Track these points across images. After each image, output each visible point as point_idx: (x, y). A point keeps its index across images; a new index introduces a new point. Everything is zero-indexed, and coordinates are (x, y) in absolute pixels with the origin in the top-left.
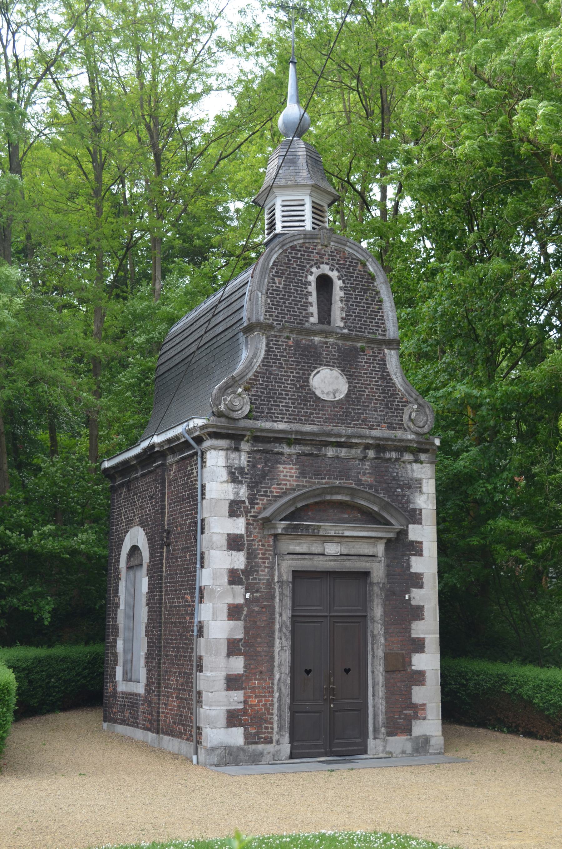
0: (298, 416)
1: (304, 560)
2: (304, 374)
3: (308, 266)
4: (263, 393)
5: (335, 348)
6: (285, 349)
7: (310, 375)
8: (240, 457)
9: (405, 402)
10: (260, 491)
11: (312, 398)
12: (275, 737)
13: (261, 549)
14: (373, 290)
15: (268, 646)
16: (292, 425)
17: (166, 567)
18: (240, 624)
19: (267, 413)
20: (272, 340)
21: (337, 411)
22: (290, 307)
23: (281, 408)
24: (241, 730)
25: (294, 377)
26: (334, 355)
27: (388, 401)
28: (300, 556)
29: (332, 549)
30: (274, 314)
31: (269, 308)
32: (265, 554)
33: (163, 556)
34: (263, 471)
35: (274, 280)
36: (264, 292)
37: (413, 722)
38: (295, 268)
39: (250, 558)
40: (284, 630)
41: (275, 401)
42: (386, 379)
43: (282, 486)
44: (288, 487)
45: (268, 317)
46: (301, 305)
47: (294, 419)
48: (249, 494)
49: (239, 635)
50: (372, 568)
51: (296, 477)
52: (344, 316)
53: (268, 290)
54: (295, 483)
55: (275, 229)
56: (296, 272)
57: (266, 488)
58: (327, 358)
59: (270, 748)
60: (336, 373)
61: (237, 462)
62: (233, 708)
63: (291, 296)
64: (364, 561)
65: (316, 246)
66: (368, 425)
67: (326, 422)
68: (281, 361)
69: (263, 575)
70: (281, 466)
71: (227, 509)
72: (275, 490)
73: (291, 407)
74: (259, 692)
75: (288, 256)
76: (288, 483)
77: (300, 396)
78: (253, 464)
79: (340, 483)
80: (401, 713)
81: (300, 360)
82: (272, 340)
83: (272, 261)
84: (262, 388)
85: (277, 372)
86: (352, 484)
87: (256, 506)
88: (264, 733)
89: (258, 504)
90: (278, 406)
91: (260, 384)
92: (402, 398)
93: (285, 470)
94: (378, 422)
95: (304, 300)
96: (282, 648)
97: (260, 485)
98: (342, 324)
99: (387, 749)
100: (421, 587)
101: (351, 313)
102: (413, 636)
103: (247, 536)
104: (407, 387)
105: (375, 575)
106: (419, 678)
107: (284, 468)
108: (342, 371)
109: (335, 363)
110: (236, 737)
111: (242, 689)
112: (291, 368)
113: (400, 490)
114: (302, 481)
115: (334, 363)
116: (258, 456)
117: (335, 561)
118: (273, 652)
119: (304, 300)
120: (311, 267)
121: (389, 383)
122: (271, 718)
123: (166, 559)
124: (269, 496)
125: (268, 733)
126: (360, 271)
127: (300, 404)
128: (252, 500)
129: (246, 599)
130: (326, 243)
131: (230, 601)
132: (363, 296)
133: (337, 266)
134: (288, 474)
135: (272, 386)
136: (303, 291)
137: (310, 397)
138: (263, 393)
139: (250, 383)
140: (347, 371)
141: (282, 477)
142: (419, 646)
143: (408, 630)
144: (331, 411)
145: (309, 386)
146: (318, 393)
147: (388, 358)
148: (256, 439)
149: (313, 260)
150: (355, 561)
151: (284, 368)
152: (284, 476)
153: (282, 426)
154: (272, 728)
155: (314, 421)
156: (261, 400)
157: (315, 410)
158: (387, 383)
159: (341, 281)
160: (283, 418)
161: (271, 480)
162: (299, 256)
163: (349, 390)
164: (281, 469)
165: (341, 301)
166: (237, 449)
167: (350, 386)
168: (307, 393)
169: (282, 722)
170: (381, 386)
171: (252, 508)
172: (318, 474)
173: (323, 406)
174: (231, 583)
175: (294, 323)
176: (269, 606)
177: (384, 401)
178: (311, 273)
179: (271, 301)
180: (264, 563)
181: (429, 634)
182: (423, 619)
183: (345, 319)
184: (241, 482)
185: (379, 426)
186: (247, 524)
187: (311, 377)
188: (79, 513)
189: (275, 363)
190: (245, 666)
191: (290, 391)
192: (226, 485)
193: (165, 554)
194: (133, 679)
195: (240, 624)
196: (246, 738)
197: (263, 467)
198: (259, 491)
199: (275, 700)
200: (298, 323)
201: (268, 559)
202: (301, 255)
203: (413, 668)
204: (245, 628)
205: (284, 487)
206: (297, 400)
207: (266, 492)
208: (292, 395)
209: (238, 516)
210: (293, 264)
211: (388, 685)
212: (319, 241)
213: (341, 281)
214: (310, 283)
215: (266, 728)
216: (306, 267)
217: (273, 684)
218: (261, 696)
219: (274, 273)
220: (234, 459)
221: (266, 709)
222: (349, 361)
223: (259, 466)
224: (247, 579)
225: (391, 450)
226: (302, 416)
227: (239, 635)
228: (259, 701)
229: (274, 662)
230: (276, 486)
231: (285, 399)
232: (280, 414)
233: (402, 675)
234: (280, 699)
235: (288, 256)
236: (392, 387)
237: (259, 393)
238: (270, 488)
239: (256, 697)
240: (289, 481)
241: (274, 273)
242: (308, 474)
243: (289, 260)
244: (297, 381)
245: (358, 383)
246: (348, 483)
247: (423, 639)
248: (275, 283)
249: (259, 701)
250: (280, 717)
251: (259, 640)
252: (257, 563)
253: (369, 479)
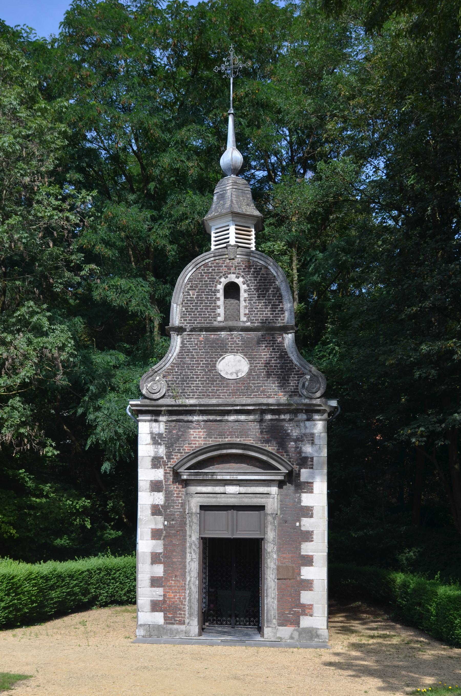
0: (206, 392)
1: (209, 497)
2: (211, 361)
3: (217, 277)
4: (178, 378)
5: (239, 338)
6: (197, 344)
7: (216, 361)
8: (159, 426)
9: (301, 374)
10: (175, 450)
11: (218, 378)
12: (187, 621)
13: (176, 491)
16: (200, 400)
18: (161, 542)
19: (181, 393)
20: (186, 339)
21: (239, 387)
22: (201, 312)
23: (192, 388)
24: (162, 614)
25: (203, 364)
26: (238, 344)
27: (285, 375)
28: (205, 495)
30: (188, 319)
31: (184, 314)
32: (179, 494)
35: (189, 292)
36: (179, 303)
37: (301, 617)
38: (207, 281)
39: (168, 496)
40: (194, 547)
42: (284, 357)
43: (192, 445)
44: (197, 445)
45: (183, 321)
46: (211, 309)
47: (203, 395)
48: (167, 452)
49: (160, 550)
50: (267, 503)
52: (247, 312)
53: (184, 301)
54: (203, 443)
56: (207, 284)
57: (179, 447)
58: (232, 347)
59: (183, 627)
60: (239, 357)
61: (157, 429)
63: (202, 303)
64: (259, 498)
65: (224, 261)
66: (266, 395)
67: (230, 395)
68: (193, 353)
69: (178, 509)
70: (192, 431)
71: (150, 463)
73: (200, 387)
74: (175, 589)
75: (201, 273)
76: (197, 443)
77: (208, 378)
78: (169, 431)
79: (240, 441)
80: (291, 610)
81: (209, 351)
82: (186, 339)
83: (187, 278)
84: (177, 375)
85: (189, 362)
86: (251, 440)
87: (172, 460)
88: (179, 617)
89: (173, 458)
90: (191, 387)
91: (176, 372)
92: (298, 371)
93: (195, 434)
94: (276, 392)
95: (213, 305)
96: (192, 559)
97: (175, 445)
98: (245, 319)
99: (278, 636)
100: (312, 517)
101: (254, 309)
102: (302, 553)
103: (165, 482)
104: (302, 362)
105: (269, 507)
106: (308, 585)
107: (194, 432)
109: (239, 350)
110: (159, 618)
111: (162, 587)
112: (201, 358)
113: (293, 443)
116: (173, 424)
117: (235, 498)
118: (185, 562)
119: (213, 305)
120: (220, 278)
121: (287, 360)
122: (184, 608)
124: (182, 453)
125: (182, 617)
126: (264, 274)
127: (209, 384)
129: (165, 526)
130: (232, 257)
131: (153, 527)
132: (266, 294)
133: (242, 274)
134: (197, 436)
135: (185, 372)
136: (213, 298)
137: (216, 378)
138: (178, 378)
139: (168, 372)
140: (249, 355)
141: (192, 439)
142: (308, 561)
144: (234, 387)
145: (215, 370)
146: (223, 374)
148: (170, 413)
149: (222, 272)
150: (252, 498)
151: (195, 358)
152: (194, 438)
153: (192, 402)
154: (185, 615)
156: (177, 384)
157: (221, 387)
158: (285, 360)
159: (246, 285)
160: (194, 395)
161: (184, 441)
162: (210, 271)
163: (250, 369)
164: (192, 433)
165: (245, 301)
167: (251, 366)
168: (214, 375)
169: (192, 610)
170: (279, 363)
173: (227, 384)
174: (153, 514)
175: (204, 323)
177: (281, 375)
179: (186, 309)
180: (178, 500)
181: (317, 552)
182: (312, 541)
183: (248, 314)
184: (160, 444)
185: (276, 395)
187: (218, 363)
189: (188, 355)
190: (165, 571)
191: (200, 375)
192: (149, 446)
195: (161, 542)
196: (165, 620)
197: (177, 432)
199: (187, 595)
200: (207, 323)
201: (180, 497)
202: (212, 270)
203: (302, 577)
205: (194, 446)
206: (206, 381)
207: (180, 450)
208: (201, 378)
209: (158, 468)
210: (205, 278)
211: (280, 589)
212: (227, 256)
213: (246, 285)
214: (218, 291)
215: (180, 614)
216: (215, 278)
217: (185, 584)
219: (189, 288)
220: (155, 427)
221: (180, 601)
222: (250, 347)
223: (174, 432)
224: (165, 511)
226: (209, 392)
227: (160, 550)
228: (175, 596)
229: (186, 569)
231: (196, 381)
232: (192, 392)
233: (294, 585)
234: (190, 595)
235: (201, 273)
236: (289, 363)
237: (175, 379)
238: (182, 447)
239: (172, 593)
241: (189, 288)
242: (214, 435)
244: (206, 367)
245: (259, 363)
246: (247, 440)
247: (312, 556)
248: (190, 295)
250: (190, 607)
251: (174, 554)
253: (266, 436)
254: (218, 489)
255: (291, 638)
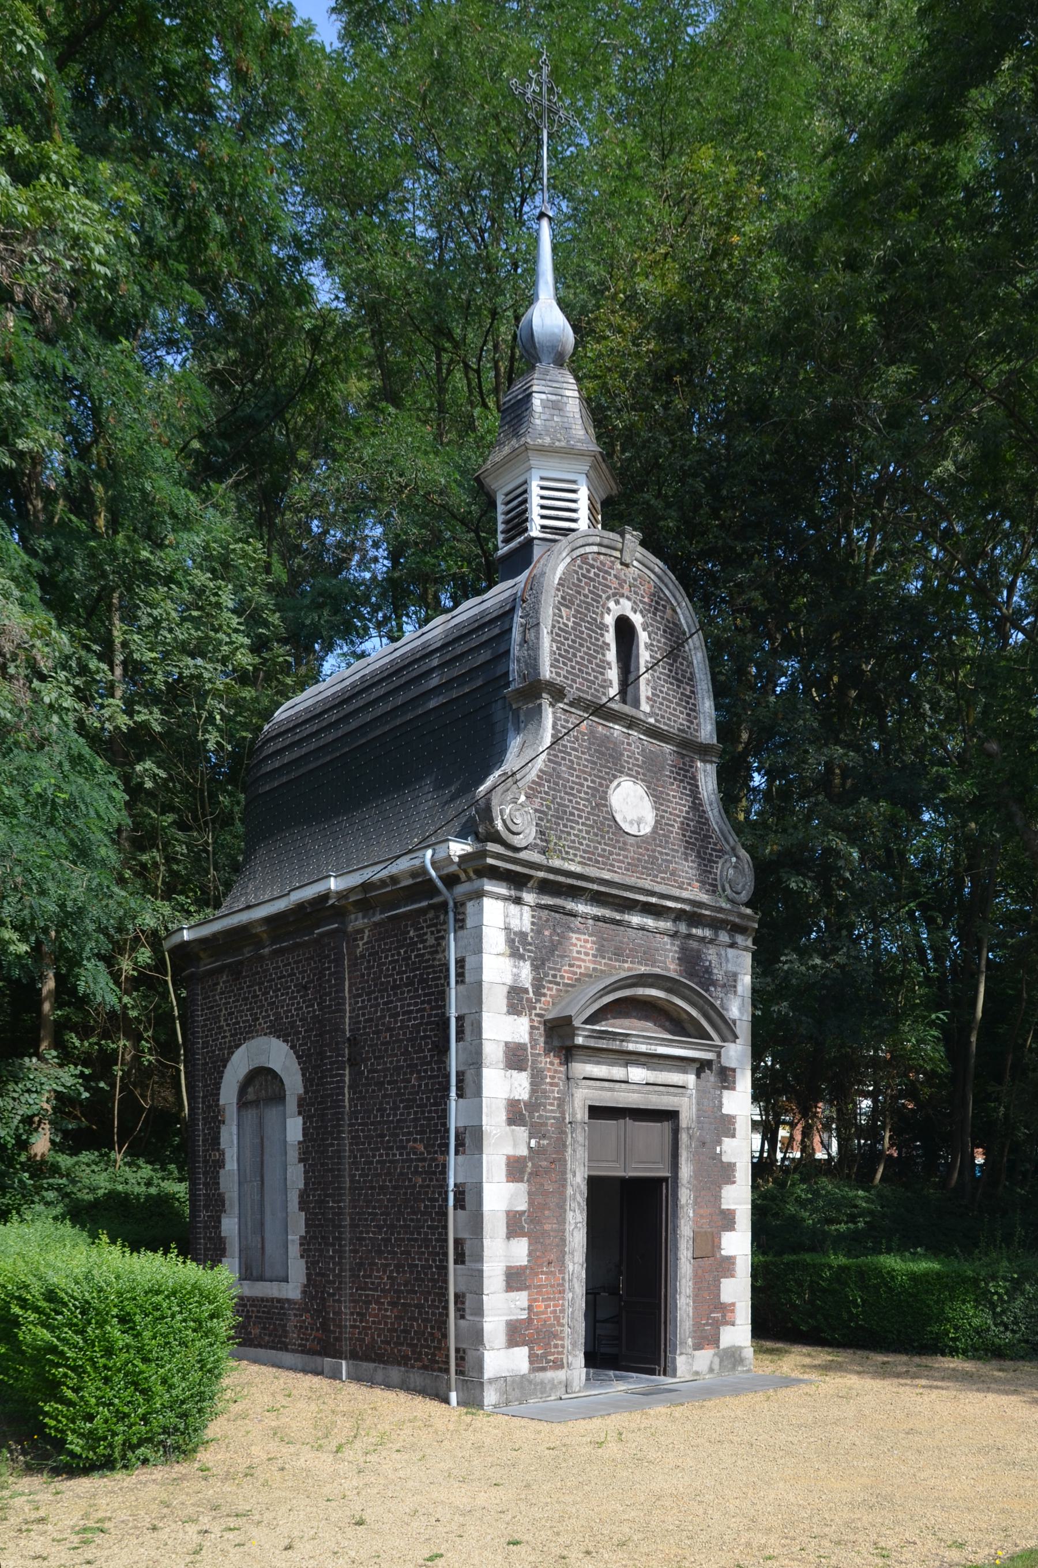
1: (602, 1089)
7: (608, 787)
13: (549, 1070)
14: (684, 658)
15: (558, 1223)
17: (351, 1100)
18: (522, 1187)
26: (637, 759)
28: (598, 1083)
29: (637, 1074)
33: (344, 1082)
34: (551, 941)
41: (565, 826)
43: (575, 969)
44: (582, 970)
47: (590, 859)
49: (522, 1206)
50: (681, 1106)
51: (594, 956)
54: (592, 966)
55: (526, 530)
59: (560, 1375)
61: (518, 922)
62: (514, 1318)
70: (574, 936)
72: (566, 975)
78: (538, 927)
88: (553, 1354)
89: (545, 995)
100: (733, 1136)
102: (724, 1207)
107: (578, 939)
108: (648, 788)
114: (600, 963)
115: (638, 773)
116: (545, 914)
120: (608, 598)
123: (350, 1087)
125: (559, 1353)
128: (538, 985)
129: (530, 1148)
131: (511, 1152)
143: (718, 1198)
147: (701, 777)
148: (545, 887)
150: (662, 1094)
155: (613, 866)
160: (575, 855)
161: (562, 957)
164: (574, 941)
166: (518, 901)
171: (538, 1001)
172: (619, 954)
176: (560, 1160)
178: (609, 610)
181: (739, 1204)
184: (521, 957)
186: (532, 1027)
187: (610, 792)
188: (816, 905)
193: (347, 1079)
194: (268, 1274)
195: (522, 1187)
196: (531, 1362)
198: (546, 975)
203: (723, 1253)
204: (530, 1193)
207: (555, 976)
215: (556, 1346)
218: (549, 1299)
225: (704, 926)
227: (522, 1206)
228: (547, 1307)
230: (567, 968)
238: (559, 970)
239: (543, 1300)
240: (584, 961)
243: (580, 580)
249: (547, 1307)
252: (544, 1091)
254: (617, 1072)
255: (711, 1370)
